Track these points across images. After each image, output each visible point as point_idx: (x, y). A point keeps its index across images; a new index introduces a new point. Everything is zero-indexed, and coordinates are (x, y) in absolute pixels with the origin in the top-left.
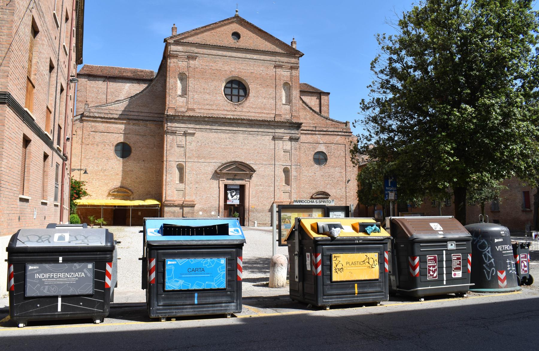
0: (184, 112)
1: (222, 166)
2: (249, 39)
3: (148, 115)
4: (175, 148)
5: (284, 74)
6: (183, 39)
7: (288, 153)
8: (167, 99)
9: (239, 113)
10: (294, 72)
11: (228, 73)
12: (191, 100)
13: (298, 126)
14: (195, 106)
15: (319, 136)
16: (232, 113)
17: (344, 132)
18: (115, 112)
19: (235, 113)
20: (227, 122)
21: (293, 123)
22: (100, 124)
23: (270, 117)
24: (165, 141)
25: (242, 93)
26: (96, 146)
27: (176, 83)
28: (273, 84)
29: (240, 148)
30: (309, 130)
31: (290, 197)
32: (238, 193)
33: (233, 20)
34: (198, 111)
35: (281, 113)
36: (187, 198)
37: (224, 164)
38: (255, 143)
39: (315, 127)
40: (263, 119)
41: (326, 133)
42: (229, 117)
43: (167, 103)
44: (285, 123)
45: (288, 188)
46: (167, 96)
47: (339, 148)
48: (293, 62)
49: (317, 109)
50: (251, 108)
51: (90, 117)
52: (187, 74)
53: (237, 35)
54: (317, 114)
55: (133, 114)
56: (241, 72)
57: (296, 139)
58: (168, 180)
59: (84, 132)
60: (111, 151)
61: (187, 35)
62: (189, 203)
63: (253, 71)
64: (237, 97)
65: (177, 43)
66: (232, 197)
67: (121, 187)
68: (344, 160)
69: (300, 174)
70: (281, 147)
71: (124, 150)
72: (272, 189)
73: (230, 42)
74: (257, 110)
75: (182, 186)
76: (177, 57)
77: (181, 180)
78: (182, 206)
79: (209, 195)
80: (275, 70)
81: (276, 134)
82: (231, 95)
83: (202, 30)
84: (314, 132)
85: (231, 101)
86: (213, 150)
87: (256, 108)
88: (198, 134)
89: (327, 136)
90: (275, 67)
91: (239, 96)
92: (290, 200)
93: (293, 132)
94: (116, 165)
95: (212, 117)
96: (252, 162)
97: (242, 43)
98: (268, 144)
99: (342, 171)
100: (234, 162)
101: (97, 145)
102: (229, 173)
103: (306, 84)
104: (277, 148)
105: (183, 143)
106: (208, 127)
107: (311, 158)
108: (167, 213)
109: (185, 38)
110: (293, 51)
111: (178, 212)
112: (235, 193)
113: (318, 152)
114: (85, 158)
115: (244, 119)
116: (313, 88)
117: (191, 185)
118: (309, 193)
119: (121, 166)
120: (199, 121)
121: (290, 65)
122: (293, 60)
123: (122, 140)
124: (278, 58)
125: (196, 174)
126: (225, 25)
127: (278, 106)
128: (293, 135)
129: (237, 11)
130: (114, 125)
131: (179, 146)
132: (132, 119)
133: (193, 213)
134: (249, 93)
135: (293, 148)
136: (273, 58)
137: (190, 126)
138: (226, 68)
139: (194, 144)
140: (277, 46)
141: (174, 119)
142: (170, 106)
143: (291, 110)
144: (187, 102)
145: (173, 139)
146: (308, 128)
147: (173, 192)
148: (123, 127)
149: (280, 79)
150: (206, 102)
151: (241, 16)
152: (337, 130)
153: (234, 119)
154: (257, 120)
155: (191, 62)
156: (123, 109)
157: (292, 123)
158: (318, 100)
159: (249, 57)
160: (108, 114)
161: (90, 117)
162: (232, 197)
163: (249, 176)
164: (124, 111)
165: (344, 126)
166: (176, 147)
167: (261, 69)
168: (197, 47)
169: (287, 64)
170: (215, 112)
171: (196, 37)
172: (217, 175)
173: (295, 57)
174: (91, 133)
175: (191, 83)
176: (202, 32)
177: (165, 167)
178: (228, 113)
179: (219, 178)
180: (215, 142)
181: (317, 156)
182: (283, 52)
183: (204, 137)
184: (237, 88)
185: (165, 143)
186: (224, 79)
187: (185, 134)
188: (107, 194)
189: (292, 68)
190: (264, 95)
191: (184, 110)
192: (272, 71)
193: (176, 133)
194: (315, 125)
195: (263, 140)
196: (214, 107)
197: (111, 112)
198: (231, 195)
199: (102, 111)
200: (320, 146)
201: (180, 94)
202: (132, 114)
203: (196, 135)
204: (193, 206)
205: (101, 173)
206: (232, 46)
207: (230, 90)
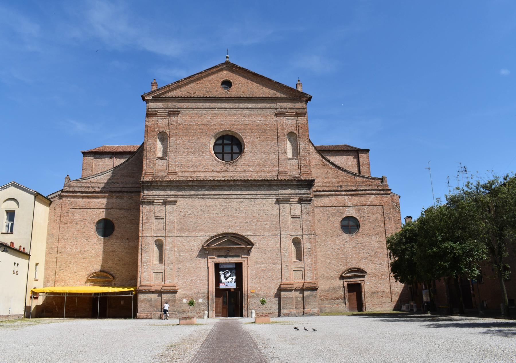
0: (163, 177)
1: (210, 239)
2: (242, 86)
3: (133, 185)
4: (153, 221)
5: (289, 122)
6: (163, 94)
7: (298, 219)
8: (145, 163)
9: (231, 174)
10: (301, 119)
11: (217, 126)
12: (172, 163)
13: (309, 184)
14: (177, 170)
15: (346, 198)
16: (223, 174)
17: (380, 190)
18: (97, 185)
19: (227, 174)
20: (216, 185)
21: (302, 180)
22: (81, 199)
23: (271, 175)
24: (141, 213)
25: (236, 149)
26: (75, 225)
27: (154, 144)
28: (274, 135)
29: (234, 217)
30: (332, 191)
31: (303, 276)
32: (234, 274)
33: (222, 67)
34: (180, 174)
35: (286, 170)
36: (168, 282)
37: (212, 237)
38: (253, 208)
39: (341, 186)
40: (263, 178)
41: (355, 192)
42: (219, 179)
43: (144, 167)
44: (292, 180)
45: (300, 265)
46: (145, 159)
47: (375, 210)
48: (298, 107)
49: (355, 170)
50: (245, 167)
51: (69, 192)
52: (168, 133)
53: (227, 84)
54: (355, 175)
55: (118, 185)
56: (233, 125)
57: (307, 200)
58: (144, 260)
59: (63, 209)
60: (91, 230)
61: (167, 89)
62: (169, 288)
63: (248, 122)
64: (230, 155)
65: (157, 99)
66: (226, 278)
67: (101, 271)
68: (383, 225)
69: (315, 246)
70: (288, 212)
71: (106, 228)
72: (278, 266)
73: (220, 91)
74: (254, 169)
75: (161, 267)
76: (156, 114)
77: (161, 260)
78: (160, 293)
79: (195, 278)
80: (275, 118)
81: (281, 196)
82: (223, 153)
83: (185, 81)
84: (339, 193)
85: (223, 160)
86: (200, 221)
87: (253, 166)
88: (181, 202)
89: (358, 197)
90: (276, 115)
91: (232, 153)
92: (303, 281)
93: (303, 192)
94: (96, 244)
95: (197, 181)
96: (249, 233)
97: (234, 92)
98: (270, 209)
99: (381, 240)
100: (225, 234)
101: (76, 223)
102: (219, 249)
103: (345, 145)
104: (282, 214)
105: (163, 214)
106: (193, 193)
107: (338, 225)
108: (142, 301)
109: (166, 92)
110: (297, 94)
111: (156, 300)
112: (229, 274)
113: (346, 217)
114: (62, 238)
115: (237, 180)
116: (350, 147)
117: (172, 266)
118: (338, 271)
119: (102, 246)
120: (181, 186)
121: (294, 111)
122: (299, 105)
123: (104, 217)
124: (279, 105)
125: (179, 252)
126: (213, 73)
127: (281, 162)
128: (304, 196)
129: (227, 57)
130: (95, 200)
131: (157, 218)
132: (115, 192)
133: (174, 301)
134: (244, 148)
135: (304, 212)
136: (274, 105)
137: (170, 193)
138: (215, 121)
139: (175, 214)
140: (277, 91)
141: (151, 185)
142: (148, 171)
143: (299, 165)
144: (168, 165)
145: (150, 210)
146: (330, 189)
147: (150, 275)
148: (104, 201)
149: (282, 129)
150: (191, 163)
151: (232, 61)
152: (370, 188)
153: (224, 180)
154: (254, 180)
155: (173, 119)
156: (106, 181)
157: (300, 181)
158: (356, 160)
159: (243, 107)
160: (89, 187)
161: (69, 192)
162: (226, 278)
163: (246, 251)
164: (107, 183)
165: (379, 183)
166: (154, 220)
167: (259, 119)
168: (179, 101)
169: (291, 111)
170: (202, 174)
171: (179, 90)
172: (205, 252)
173: (301, 102)
174: (70, 210)
175: (172, 142)
176: (186, 84)
177: (140, 243)
178: (218, 174)
179: (208, 255)
180: (201, 210)
181: (346, 223)
182: (285, 96)
183: (188, 204)
184: (229, 145)
185: (141, 215)
186: (213, 134)
187: (165, 203)
188: (85, 279)
189: (297, 114)
190: (263, 150)
191: (163, 174)
192: (272, 120)
193: (153, 202)
194: (341, 184)
195: (264, 204)
196: (200, 168)
197: (93, 185)
198: (225, 277)
199: (83, 185)
200: (348, 209)
201: (161, 156)
202: (115, 185)
203: (178, 204)
204: (174, 292)
205: (80, 256)
206: (222, 96)
207: (221, 147)
